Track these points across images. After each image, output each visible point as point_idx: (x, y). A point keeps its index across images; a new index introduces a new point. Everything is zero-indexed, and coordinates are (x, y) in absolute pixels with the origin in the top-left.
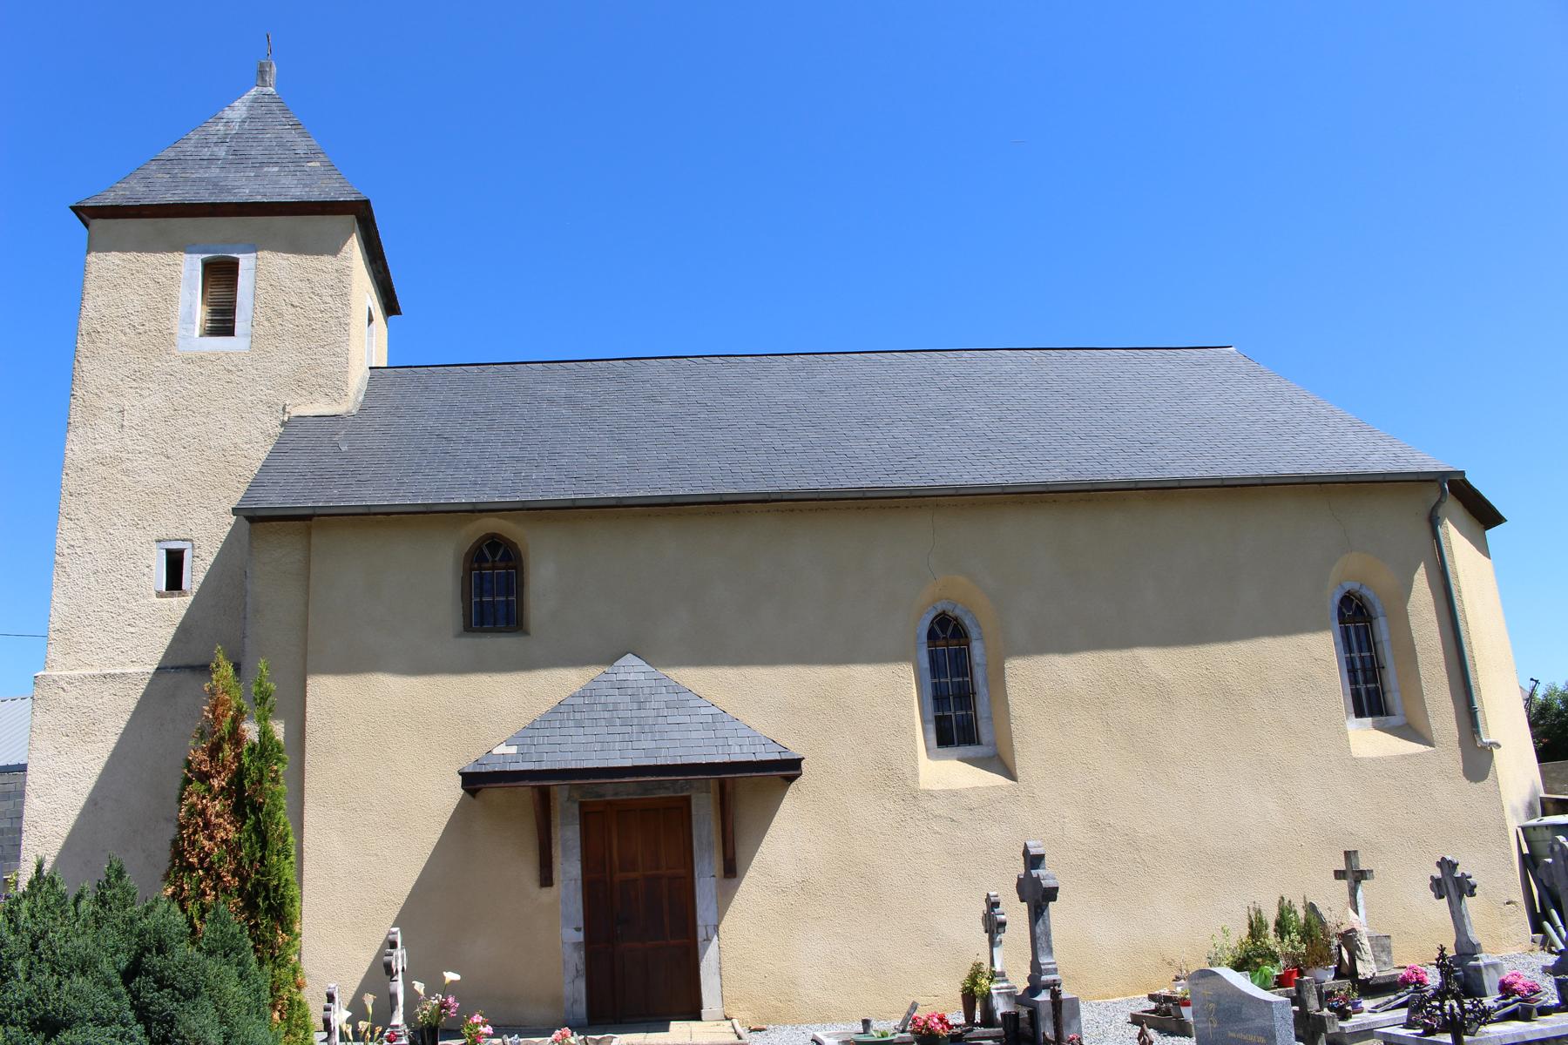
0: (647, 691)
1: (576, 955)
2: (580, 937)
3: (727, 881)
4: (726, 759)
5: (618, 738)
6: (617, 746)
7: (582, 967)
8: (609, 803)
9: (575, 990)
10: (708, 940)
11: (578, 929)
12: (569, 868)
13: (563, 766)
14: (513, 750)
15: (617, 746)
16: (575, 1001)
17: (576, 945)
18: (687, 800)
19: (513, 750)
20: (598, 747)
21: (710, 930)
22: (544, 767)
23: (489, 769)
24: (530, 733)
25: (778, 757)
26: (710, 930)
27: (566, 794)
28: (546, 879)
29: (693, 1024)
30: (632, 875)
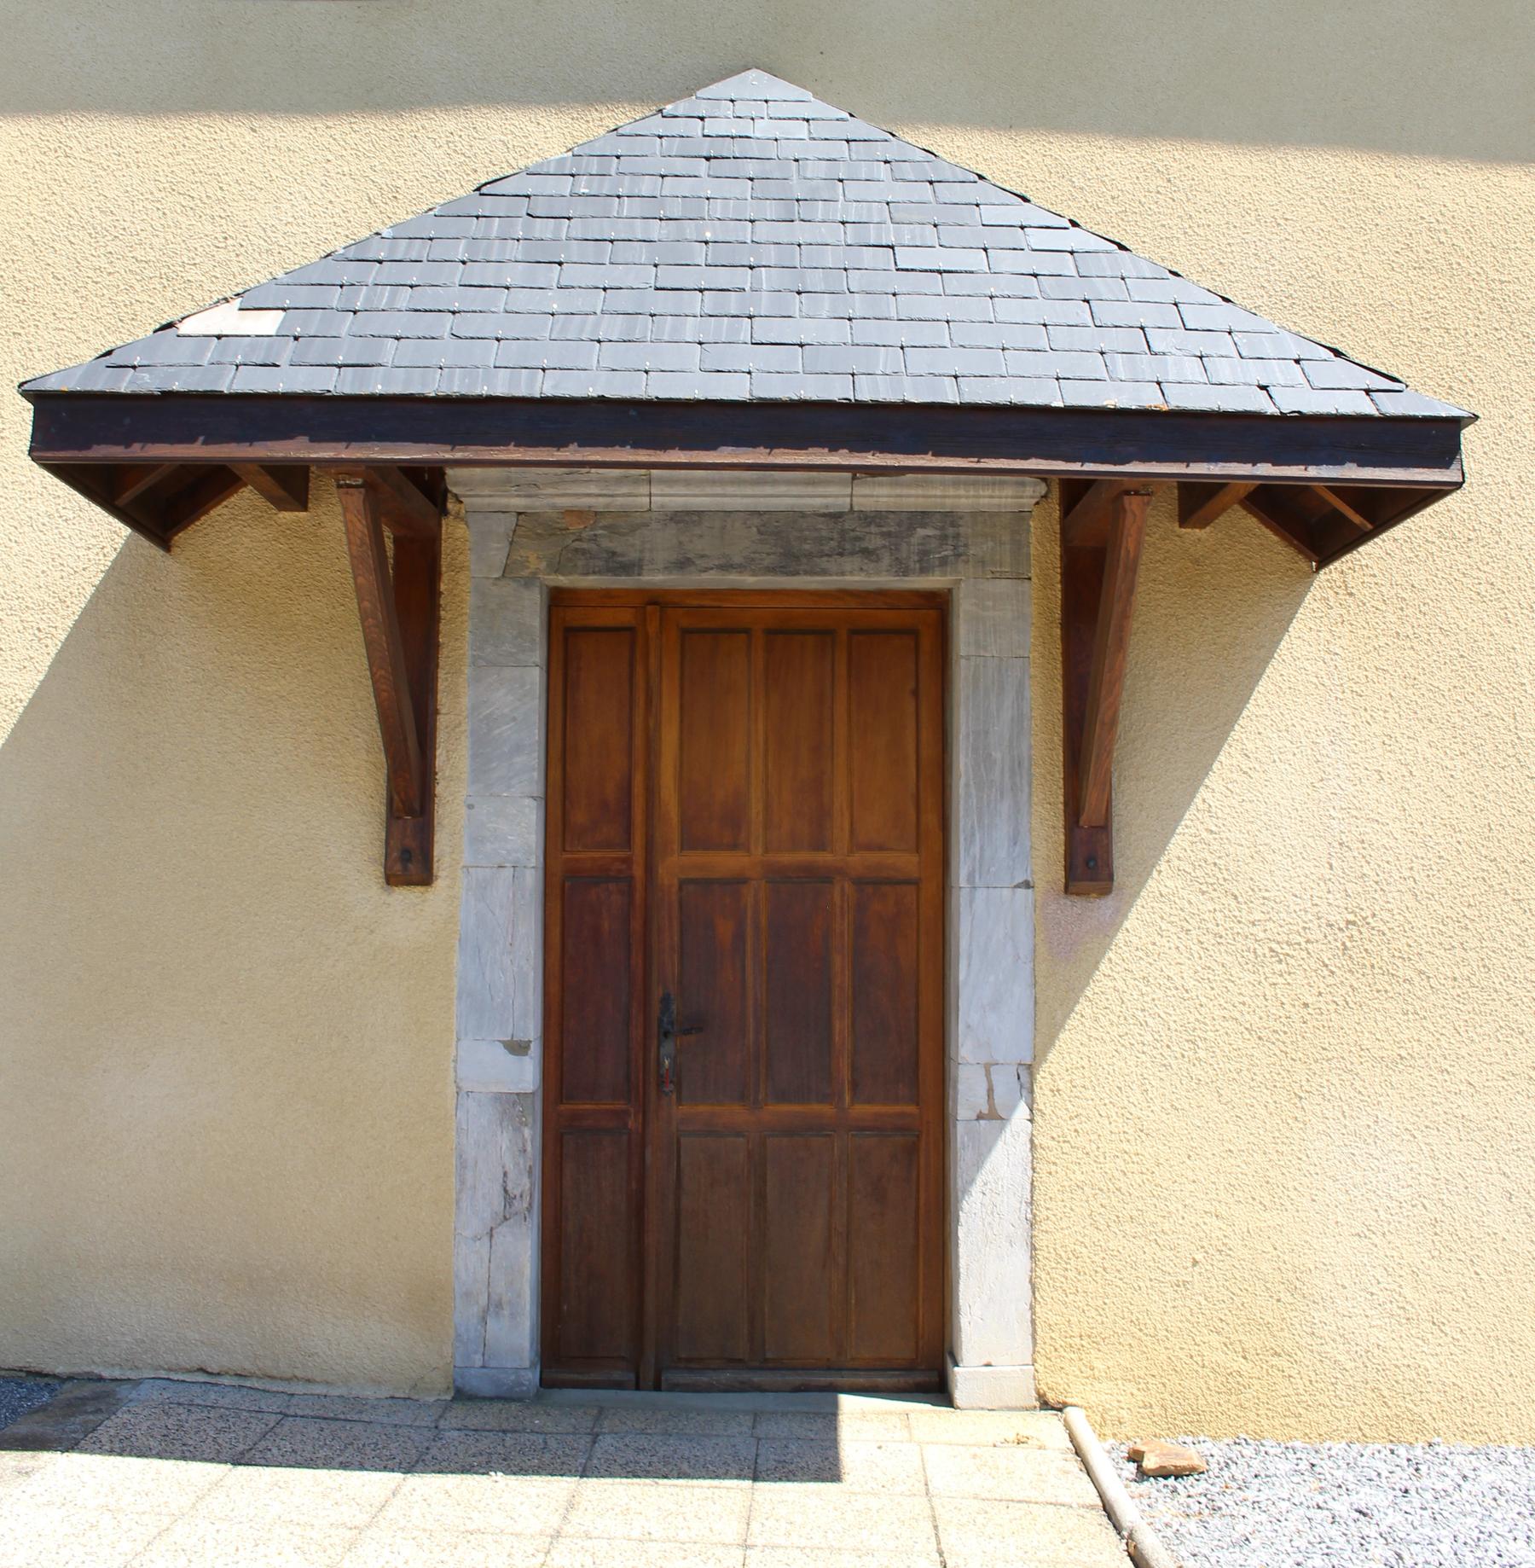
0: (815, 169)
1: (504, 1140)
2: (526, 1074)
3: (1077, 906)
4: (1149, 399)
5: (695, 302)
6: (690, 329)
7: (527, 1185)
8: (656, 601)
9: (492, 1274)
10: (994, 1116)
11: (517, 1048)
12: (495, 818)
13: (457, 385)
14: (268, 323)
15: (690, 329)
16: (494, 1306)
17: (510, 1103)
18: (939, 605)
19: (268, 323)
20: (613, 327)
21: (1004, 1081)
22: (376, 385)
23: (147, 383)
24: (349, 272)
25: (1365, 407)
26: (1004, 1081)
27: (497, 553)
28: (410, 858)
29: (921, 1412)
30: (725, 862)
